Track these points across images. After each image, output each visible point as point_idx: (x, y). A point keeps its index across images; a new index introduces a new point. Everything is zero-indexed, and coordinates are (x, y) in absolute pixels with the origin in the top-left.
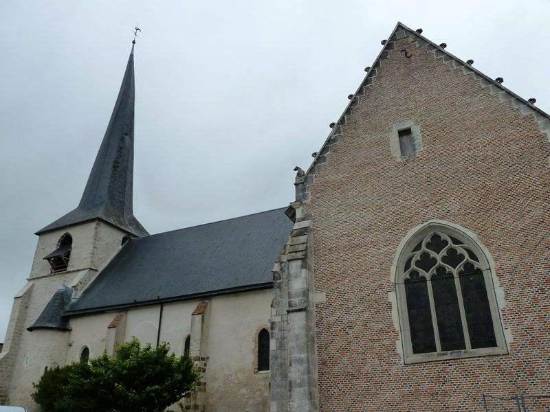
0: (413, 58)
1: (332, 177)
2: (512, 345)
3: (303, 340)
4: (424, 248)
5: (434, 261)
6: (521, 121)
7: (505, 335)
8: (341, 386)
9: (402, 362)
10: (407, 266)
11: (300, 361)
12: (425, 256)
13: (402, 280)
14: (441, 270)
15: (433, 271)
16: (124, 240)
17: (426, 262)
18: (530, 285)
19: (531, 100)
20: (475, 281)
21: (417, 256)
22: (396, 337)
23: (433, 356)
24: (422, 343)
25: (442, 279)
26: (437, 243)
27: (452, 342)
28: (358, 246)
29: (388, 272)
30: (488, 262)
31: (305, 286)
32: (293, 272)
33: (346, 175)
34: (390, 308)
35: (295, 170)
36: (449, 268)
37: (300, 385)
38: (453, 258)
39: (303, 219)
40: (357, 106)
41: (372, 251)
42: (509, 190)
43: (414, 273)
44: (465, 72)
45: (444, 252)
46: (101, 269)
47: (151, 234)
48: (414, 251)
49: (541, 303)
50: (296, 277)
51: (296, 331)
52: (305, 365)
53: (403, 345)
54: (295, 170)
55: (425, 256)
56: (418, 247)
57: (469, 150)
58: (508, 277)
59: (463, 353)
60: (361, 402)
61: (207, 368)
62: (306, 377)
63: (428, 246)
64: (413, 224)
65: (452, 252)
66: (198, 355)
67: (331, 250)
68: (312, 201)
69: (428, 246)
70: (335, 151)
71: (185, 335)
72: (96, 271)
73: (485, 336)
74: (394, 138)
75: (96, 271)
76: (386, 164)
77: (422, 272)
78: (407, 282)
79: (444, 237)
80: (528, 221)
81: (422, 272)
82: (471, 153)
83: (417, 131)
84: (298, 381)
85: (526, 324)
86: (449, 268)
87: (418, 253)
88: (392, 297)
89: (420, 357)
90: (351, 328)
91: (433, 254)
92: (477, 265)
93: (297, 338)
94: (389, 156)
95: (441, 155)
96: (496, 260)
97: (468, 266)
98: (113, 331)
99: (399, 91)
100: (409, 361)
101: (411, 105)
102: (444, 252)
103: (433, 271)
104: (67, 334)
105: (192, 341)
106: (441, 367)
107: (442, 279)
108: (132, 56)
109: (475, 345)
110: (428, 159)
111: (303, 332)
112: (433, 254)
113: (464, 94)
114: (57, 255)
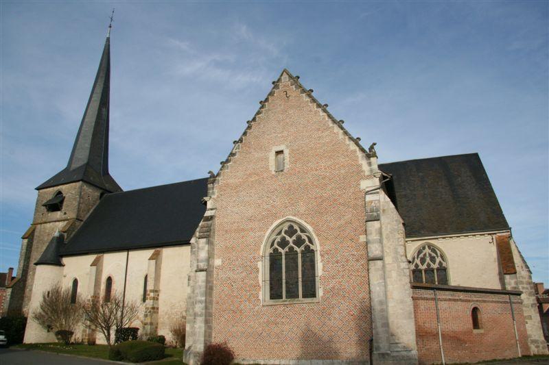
0: (291, 98)
1: (231, 181)
2: (322, 297)
3: (203, 289)
4: (283, 234)
5: (288, 243)
6: (349, 153)
7: (320, 292)
8: (226, 317)
9: (261, 304)
10: (272, 245)
11: (201, 302)
12: (283, 239)
13: (267, 254)
14: (291, 249)
15: (287, 249)
16: (102, 195)
17: (283, 243)
18: (337, 262)
19: (358, 138)
20: (309, 254)
21: (278, 239)
22: (259, 290)
23: (279, 302)
24: (275, 294)
25: (292, 255)
26: (291, 231)
27: (292, 294)
28: (243, 230)
29: (259, 249)
30: (317, 247)
31: (207, 255)
32: (200, 246)
33: (240, 180)
34: (258, 271)
35: (209, 173)
36: (296, 248)
37: (200, 316)
38: (299, 242)
39: (212, 209)
40: (252, 130)
41: (252, 234)
42: (335, 200)
43: (276, 250)
44: (322, 113)
45: (294, 238)
46: (85, 219)
47: (125, 188)
48: (277, 235)
49: (341, 274)
50: (203, 249)
51: (200, 283)
52: (204, 304)
53: (264, 293)
54: (209, 173)
55: (283, 239)
56: (280, 233)
57: (316, 170)
58: (326, 256)
59: (296, 301)
60: (237, 326)
61: (160, 298)
62: (204, 311)
63: (286, 232)
64: (276, 218)
65: (299, 237)
66: (153, 288)
67: (226, 231)
68: (218, 197)
69: (286, 232)
70: (235, 162)
71: (145, 274)
72: (82, 221)
73: (310, 292)
74: (272, 156)
75: (82, 221)
76: (265, 175)
77: (280, 250)
78: (271, 255)
79: (296, 227)
80: (342, 222)
81: (280, 250)
82: (316, 173)
83: (286, 152)
84: (199, 313)
85: (331, 286)
86: (296, 248)
87: (279, 237)
88: (260, 265)
89: (272, 302)
90: (235, 282)
91: (288, 238)
92: (312, 247)
93: (200, 287)
94: (267, 169)
95: (299, 172)
96: (321, 245)
97: (307, 248)
98: (94, 268)
99: (279, 122)
100: (265, 304)
101: (285, 133)
102: (294, 238)
103: (287, 249)
104: (62, 267)
105: (148, 279)
106: (282, 308)
107: (292, 255)
108: (108, 40)
109: (305, 296)
110: (291, 174)
111: (204, 284)
112: (288, 238)
113: (319, 130)
114: (54, 202)
